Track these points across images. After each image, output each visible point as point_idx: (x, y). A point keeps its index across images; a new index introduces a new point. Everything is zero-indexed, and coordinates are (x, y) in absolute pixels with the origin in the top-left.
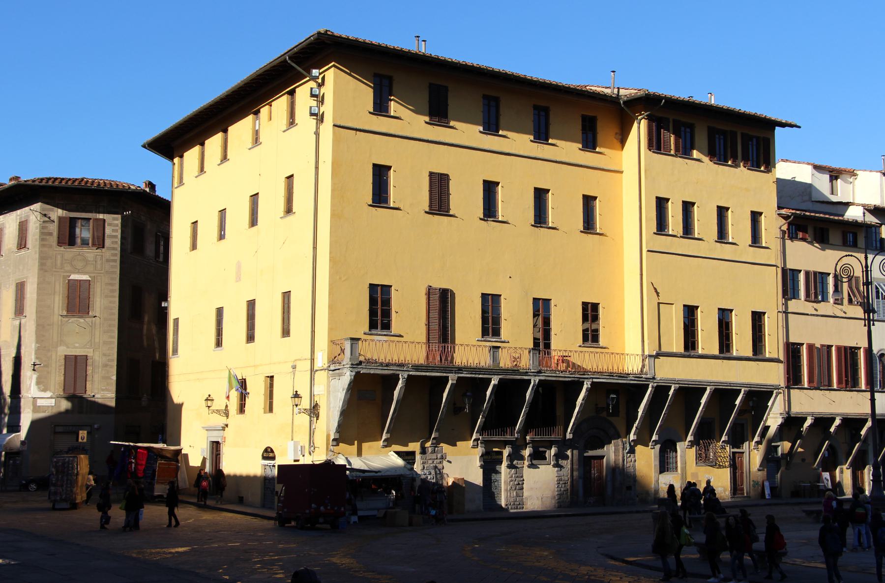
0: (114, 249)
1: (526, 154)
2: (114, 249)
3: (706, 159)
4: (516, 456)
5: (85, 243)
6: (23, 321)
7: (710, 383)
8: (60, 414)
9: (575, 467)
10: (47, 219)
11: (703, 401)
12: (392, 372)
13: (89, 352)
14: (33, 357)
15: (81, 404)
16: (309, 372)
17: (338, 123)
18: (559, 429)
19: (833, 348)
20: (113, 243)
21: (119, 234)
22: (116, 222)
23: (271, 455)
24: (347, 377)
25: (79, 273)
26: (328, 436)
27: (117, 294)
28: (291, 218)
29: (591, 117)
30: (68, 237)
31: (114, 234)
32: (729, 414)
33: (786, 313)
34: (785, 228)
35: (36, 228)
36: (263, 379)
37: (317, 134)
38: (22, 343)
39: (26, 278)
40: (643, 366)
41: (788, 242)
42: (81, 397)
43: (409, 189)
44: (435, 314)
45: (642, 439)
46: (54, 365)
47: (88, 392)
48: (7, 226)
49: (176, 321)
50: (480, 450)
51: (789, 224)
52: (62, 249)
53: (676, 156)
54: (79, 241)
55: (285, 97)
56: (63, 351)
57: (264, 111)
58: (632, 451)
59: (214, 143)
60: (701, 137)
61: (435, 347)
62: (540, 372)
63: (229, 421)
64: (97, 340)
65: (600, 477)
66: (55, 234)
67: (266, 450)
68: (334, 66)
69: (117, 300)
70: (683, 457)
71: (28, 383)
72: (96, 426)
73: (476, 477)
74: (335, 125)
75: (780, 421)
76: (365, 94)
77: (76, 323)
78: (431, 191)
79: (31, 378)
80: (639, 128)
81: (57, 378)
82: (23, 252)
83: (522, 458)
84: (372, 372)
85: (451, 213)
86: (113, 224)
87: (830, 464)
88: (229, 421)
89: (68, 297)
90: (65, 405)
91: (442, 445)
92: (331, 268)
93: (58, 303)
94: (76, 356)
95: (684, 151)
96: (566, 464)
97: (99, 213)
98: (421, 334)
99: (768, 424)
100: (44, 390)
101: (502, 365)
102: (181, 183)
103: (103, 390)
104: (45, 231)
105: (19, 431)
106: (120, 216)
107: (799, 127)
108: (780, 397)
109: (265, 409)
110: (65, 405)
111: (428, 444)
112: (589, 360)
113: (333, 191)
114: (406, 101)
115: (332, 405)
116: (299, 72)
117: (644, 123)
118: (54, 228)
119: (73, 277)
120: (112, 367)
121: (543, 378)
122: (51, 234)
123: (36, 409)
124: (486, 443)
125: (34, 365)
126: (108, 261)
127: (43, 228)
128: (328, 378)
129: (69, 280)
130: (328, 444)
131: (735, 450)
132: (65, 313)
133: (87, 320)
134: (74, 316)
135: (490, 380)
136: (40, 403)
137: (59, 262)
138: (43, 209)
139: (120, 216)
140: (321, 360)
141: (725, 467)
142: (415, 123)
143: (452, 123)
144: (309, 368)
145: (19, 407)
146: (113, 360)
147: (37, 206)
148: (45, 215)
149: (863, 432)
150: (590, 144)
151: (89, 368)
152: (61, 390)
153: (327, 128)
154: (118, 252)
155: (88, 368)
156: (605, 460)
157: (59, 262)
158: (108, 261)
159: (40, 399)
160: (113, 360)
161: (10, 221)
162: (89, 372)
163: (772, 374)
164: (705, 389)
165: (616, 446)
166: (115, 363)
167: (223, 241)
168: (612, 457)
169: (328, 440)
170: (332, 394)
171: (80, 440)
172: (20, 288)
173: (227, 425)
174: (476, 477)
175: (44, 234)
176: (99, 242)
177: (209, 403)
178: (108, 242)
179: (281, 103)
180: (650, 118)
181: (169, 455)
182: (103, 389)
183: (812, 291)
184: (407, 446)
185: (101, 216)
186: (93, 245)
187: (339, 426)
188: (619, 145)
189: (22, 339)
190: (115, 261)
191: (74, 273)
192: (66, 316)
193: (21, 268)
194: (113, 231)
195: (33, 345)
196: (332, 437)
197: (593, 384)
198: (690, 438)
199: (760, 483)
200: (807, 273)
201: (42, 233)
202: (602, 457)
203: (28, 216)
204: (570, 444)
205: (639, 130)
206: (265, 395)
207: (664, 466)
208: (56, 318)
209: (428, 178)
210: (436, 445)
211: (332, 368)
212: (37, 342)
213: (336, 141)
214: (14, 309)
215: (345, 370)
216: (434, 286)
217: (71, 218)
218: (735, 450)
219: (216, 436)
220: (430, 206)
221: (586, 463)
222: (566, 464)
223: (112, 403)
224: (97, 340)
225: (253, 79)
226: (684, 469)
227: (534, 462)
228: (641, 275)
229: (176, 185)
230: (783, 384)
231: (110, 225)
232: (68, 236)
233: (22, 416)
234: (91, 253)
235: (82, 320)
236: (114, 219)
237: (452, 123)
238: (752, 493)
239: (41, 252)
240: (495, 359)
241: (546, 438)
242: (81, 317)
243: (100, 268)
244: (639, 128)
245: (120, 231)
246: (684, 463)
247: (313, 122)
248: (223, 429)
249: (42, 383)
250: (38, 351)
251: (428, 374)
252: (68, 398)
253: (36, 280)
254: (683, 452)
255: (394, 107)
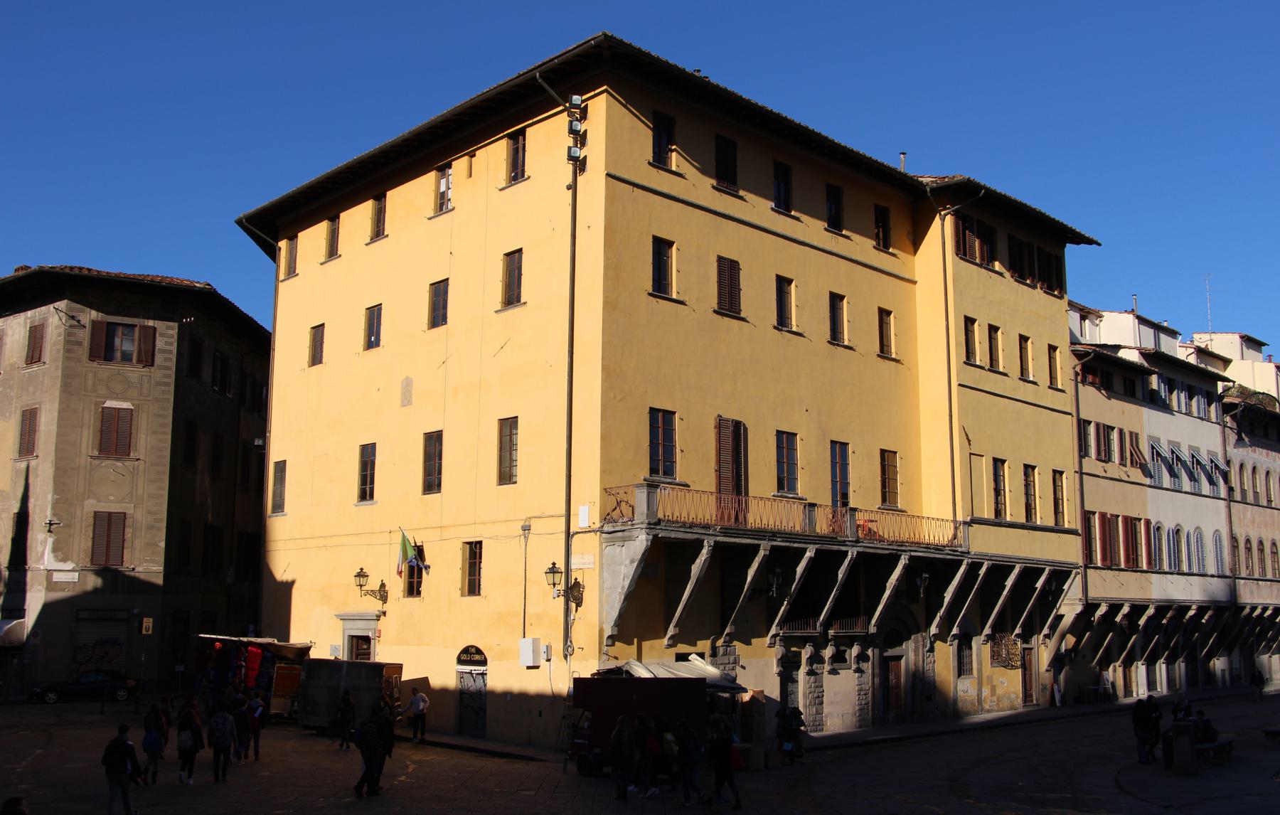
0: (167, 368)
1: (821, 246)
2: (167, 368)
3: (1007, 275)
4: (816, 659)
5: (126, 358)
6: (33, 463)
7: (1047, 563)
8: (86, 595)
9: (877, 671)
10: (75, 323)
11: (1009, 583)
12: (696, 536)
13: (128, 508)
14: (49, 513)
15: (115, 581)
16: (563, 536)
17: (613, 172)
18: (861, 620)
19: (1120, 519)
20: (166, 359)
21: (174, 348)
22: (171, 332)
23: (477, 657)
24: (640, 542)
25: (117, 399)
26: (601, 631)
27: (169, 429)
28: (514, 312)
29: (882, 203)
30: (103, 349)
31: (167, 348)
32: (1008, 599)
33: (1081, 473)
34: (1078, 369)
35: (59, 335)
36: (460, 546)
37: (573, 187)
38: (31, 493)
39: (40, 403)
40: (955, 537)
41: (1080, 385)
42: (117, 571)
43: (693, 277)
44: (728, 457)
45: (942, 636)
46: (78, 525)
47: (126, 564)
48: (10, 333)
49: (281, 466)
50: (778, 650)
51: (1083, 366)
52: (95, 364)
53: (980, 266)
54: (118, 355)
55: (504, 142)
56: (91, 505)
57: (460, 165)
58: (932, 650)
59: (357, 219)
60: (1002, 246)
61: (729, 498)
62: (857, 541)
63: (386, 607)
64: (140, 492)
65: (898, 684)
66: (86, 344)
67: (466, 650)
68: (605, 91)
69: (169, 437)
70: (979, 655)
71: (40, 549)
72: (136, 611)
73: (774, 691)
74: (608, 175)
75: (1079, 608)
76: (642, 137)
77: (110, 468)
78: (720, 283)
79: (45, 542)
80: (943, 225)
81: (83, 542)
82: (35, 368)
83: (822, 661)
84: (673, 535)
85: (743, 315)
86: (167, 335)
87: (1106, 662)
88: (386, 607)
89: (101, 431)
90: (93, 582)
91: (735, 643)
92: (604, 381)
93: (87, 439)
94: (110, 514)
95: (986, 263)
96: (868, 667)
97: (148, 318)
98: (710, 483)
99: (1061, 612)
100: (64, 560)
101: (818, 530)
102: (292, 272)
103: (146, 561)
104: (73, 339)
105: (23, 617)
106: (176, 325)
107: (1099, 245)
108: (1079, 577)
109: (462, 589)
110: (93, 582)
111: (720, 643)
112: (889, 528)
113: (606, 268)
114: (691, 154)
115: (606, 585)
116: (552, 97)
117: (949, 220)
118: (84, 336)
119: (109, 404)
120: (159, 529)
121: (861, 549)
122: (80, 344)
123: (51, 586)
124: (787, 641)
125: (51, 524)
126: (158, 384)
127: (68, 334)
128: (601, 544)
129: (103, 409)
130: (600, 643)
131: (1026, 646)
132: (96, 453)
133: (127, 463)
134: (108, 458)
135: (804, 550)
136: (57, 577)
137: (90, 383)
138: (69, 309)
139: (176, 325)
140: (587, 514)
141: (1017, 668)
142: (701, 187)
143: (742, 193)
144: (563, 528)
145: (24, 583)
146: (161, 520)
147: (62, 304)
148: (73, 318)
149: (1142, 622)
150: (884, 244)
151: (128, 531)
152: (88, 559)
153: (594, 183)
154: (172, 373)
155: (127, 530)
156: (903, 661)
157: (90, 383)
158: (158, 384)
159: (55, 571)
160: (161, 520)
161: (16, 327)
162: (128, 536)
163: (1068, 550)
164: (1013, 567)
165: (916, 642)
166: (165, 524)
167: (374, 351)
168: (912, 656)
169: (601, 637)
170: (608, 572)
171: (144, 632)
172: (29, 420)
173: (384, 613)
174: (774, 691)
175: (70, 342)
176: (147, 358)
177: (363, 581)
178: (159, 359)
179: (495, 154)
180: (957, 215)
181: (290, 656)
182: (146, 561)
183: (1103, 448)
184: (695, 645)
185: (151, 323)
186: (139, 361)
187: (620, 616)
188: (910, 247)
189: (31, 488)
190: (168, 384)
191: (111, 399)
192: (98, 458)
193: (31, 389)
194: (167, 343)
195: (50, 497)
196: (608, 632)
197: (911, 558)
198: (987, 630)
199: (1049, 687)
200: (1098, 425)
201: (67, 342)
202: (900, 657)
203: (46, 319)
204: (866, 641)
205: (941, 230)
206: (463, 569)
207: (962, 668)
208: (83, 460)
209: (715, 265)
210: (728, 644)
211: (608, 528)
212: (55, 492)
213: (610, 199)
214: (17, 447)
215: (635, 533)
216: (724, 416)
217: (109, 323)
218: (1026, 646)
219: (359, 629)
220: (719, 303)
221: (886, 665)
222: (868, 667)
223: (159, 580)
224: (140, 493)
225: (501, 93)
226: (980, 670)
227: (836, 665)
228: (951, 416)
229: (282, 277)
230: (1081, 563)
231: (162, 335)
232: (103, 347)
233: (29, 596)
234: (135, 372)
235: (119, 464)
236: (169, 328)
237: (742, 193)
238: (1041, 701)
239: (65, 368)
240: (811, 522)
241: (798, 633)
242: (118, 460)
243: (145, 395)
244: (943, 225)
245: (176, 344)
246: (980, 664)
247: (569, 168)
248: (378, 618)
249: (60, 551)
250: (56, 505)
251: (737, 540)
252: (98, 573)
253: (57, 406)
254: (979, 649)
255: (675, 160)
